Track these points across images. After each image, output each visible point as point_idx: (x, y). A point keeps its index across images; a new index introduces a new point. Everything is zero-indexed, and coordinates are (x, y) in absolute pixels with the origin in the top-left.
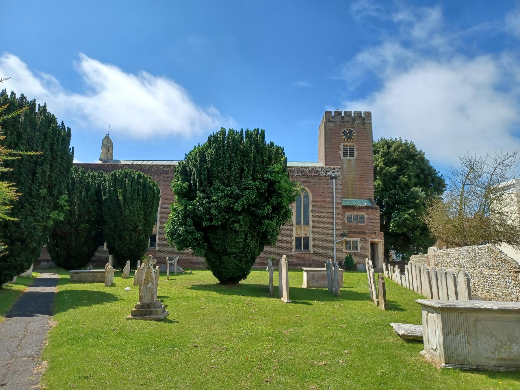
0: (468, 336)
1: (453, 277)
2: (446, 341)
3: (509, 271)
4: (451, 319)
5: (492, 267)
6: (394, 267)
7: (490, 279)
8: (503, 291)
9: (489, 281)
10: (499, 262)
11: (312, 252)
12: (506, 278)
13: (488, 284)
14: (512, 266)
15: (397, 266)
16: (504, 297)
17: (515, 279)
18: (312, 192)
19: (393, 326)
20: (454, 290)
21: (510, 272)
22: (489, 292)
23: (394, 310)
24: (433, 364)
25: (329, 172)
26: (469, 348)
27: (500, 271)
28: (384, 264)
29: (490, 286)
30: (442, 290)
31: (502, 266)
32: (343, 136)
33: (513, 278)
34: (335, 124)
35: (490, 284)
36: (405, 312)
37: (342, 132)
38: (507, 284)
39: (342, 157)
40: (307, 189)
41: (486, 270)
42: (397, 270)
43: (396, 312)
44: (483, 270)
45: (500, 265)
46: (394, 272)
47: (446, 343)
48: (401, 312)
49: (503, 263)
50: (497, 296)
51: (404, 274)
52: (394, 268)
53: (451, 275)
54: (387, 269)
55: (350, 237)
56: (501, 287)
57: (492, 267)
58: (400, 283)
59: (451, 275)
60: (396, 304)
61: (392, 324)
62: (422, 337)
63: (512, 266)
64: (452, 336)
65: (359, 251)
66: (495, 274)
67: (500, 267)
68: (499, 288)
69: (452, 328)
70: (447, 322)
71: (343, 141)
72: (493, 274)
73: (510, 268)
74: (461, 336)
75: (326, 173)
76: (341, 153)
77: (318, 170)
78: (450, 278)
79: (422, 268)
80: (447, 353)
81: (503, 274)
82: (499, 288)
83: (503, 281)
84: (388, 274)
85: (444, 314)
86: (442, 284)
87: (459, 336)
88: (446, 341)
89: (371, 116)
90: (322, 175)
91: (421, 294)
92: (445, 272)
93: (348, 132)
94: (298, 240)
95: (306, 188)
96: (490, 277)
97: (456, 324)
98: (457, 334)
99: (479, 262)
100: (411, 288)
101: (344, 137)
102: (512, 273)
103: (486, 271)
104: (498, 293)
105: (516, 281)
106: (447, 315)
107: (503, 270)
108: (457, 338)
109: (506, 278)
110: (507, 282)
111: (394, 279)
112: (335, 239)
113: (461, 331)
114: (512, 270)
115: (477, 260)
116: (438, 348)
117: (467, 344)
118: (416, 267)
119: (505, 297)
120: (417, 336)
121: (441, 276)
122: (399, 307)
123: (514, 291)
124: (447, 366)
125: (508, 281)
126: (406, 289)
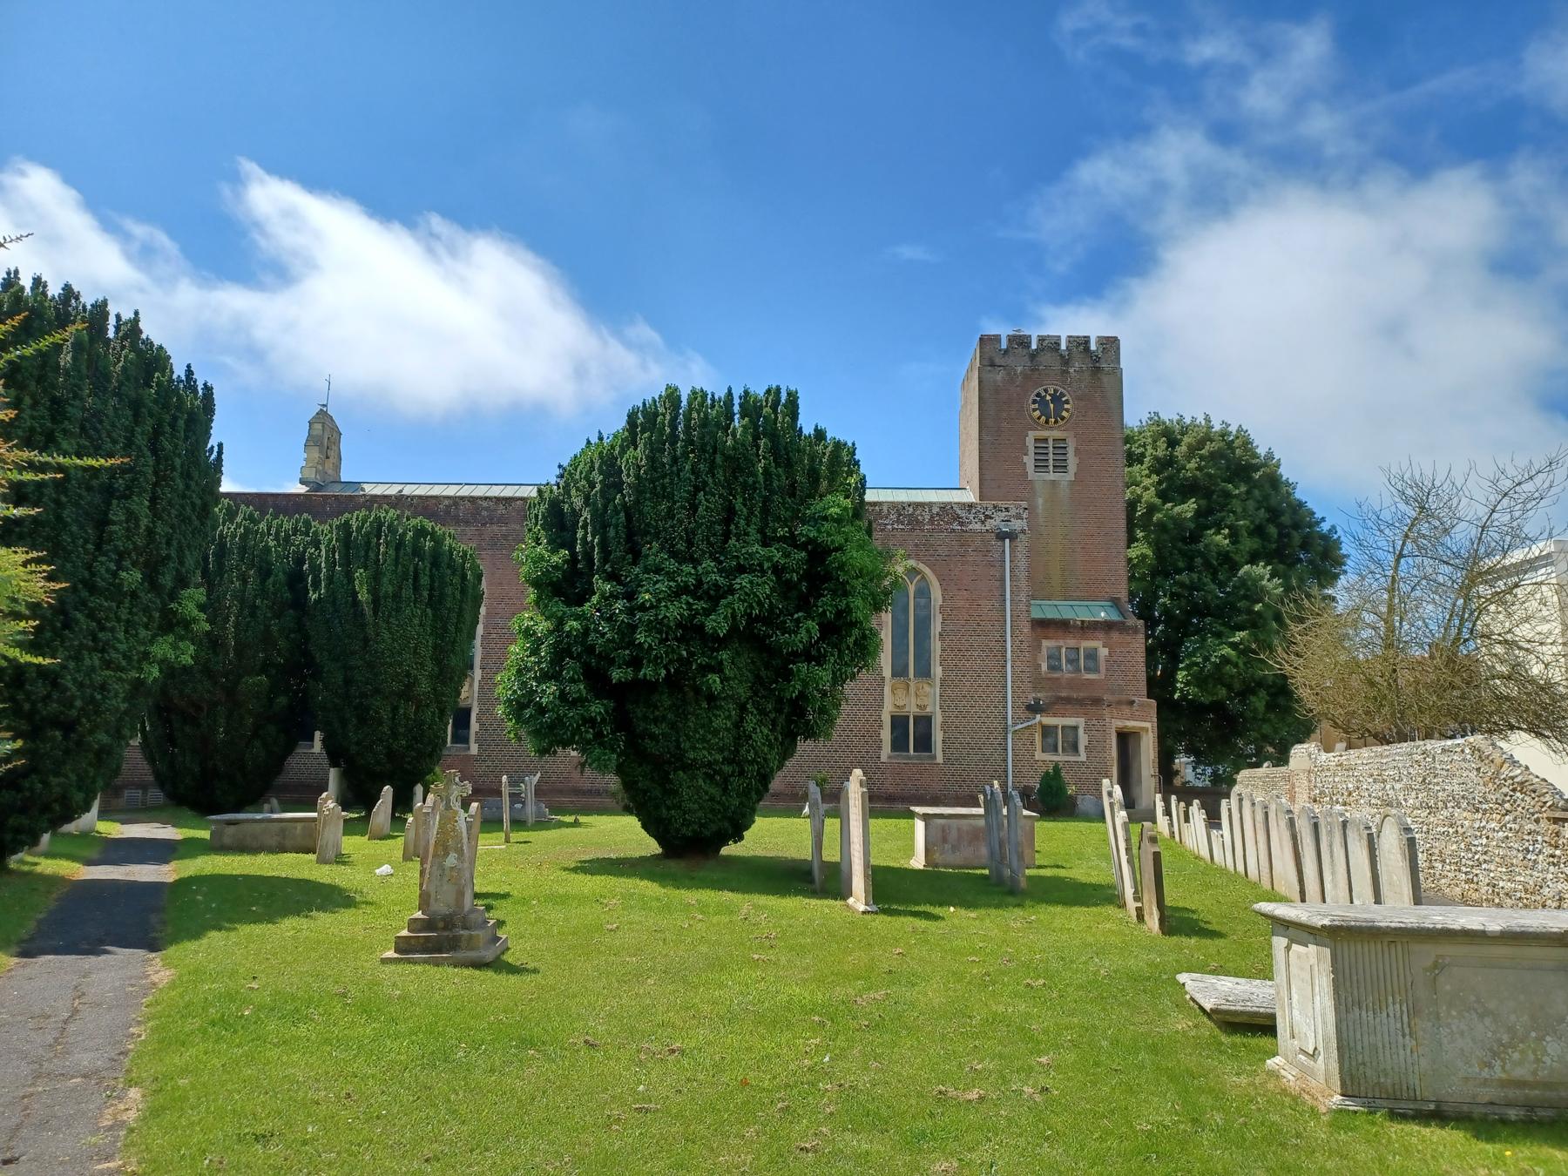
0: (1412, 1012)
1: (1365, 837)
2: (1344, 1028)
3: (1536, 816)
4: (1360, 960)
5: (1484, 806)
6: (1189, 804)
7: (1476, 843)
8: (1518, 878)
9: (1473, 849)
10: (1505, 790)
11: (940, 759)
12: (1526, 837)
13: (1470, 855)
14: (1545, 803)
15: (1196, 802)
16: (1518, 895)
17: (1553, 842)
18: (941, 580)
19: (1184, 984)
20: (1369, 874)
21: (1537, 821)
22: (1475, 879)
23: (1188, 935)
24: (1306, 1097)
25: (992, 518)
26: (1414, 1049)
27: (1507, 818)
28: (1159, 796)
29: (1476, 863)
30: (1333, 873)
31: (1515, 801)
32: (1034, 410)
33: (1546, 839)
34: (1009, 374)
35: (1477, 857)
36: (1222, 940)
37: (1033, 397)
38: (1529, 857)
39: (1031, 473)
40: (927, 571)
41: (1465, 814)
42: (1198, 814)
43: (1193, 941)
44: (1456, 815)
45: (1508, 798)
46: (1187, 820)
47: (1345, 1035)
48: (1208, 942)
49: (1518, 794)
50: (1498, 894)
51: (1219, 826)
52: (1187, 808)
53: (1359, 830)
54: (1168, 812)
55: (1055, 715)
56: (1512, 864)
57: (1484, 806)
58: (1205, 853)
59: (1359, 830)
60: (1195, 917)
61: (1182, 978)
62: (1273, 1017)
63: (1545, 803)
64: (1364, 1013)
65: (1083, 757)
66: (1493, 825)
67: (1507, 806)
68: (1504, 870)
69: (1362, 990)
70: (1347, 971)
71: (1035, 424)
72: (1488, 826)
73: (1537, 809)
74: (1391, 1015)
75: (983, 522)
76: (1029, 460)
77: (959, 512)
78: (1357, 838)
79: (1273, 807)
80: (1346, 1065)
81: (1517, 827)
82: (1504, 870)
83: (1516, 846)
84: (1171, 825)
85: (1339, 947)
86: (1332, 856)
87: (1385, 1014)
88: (1344, 1028)
89: (1119, 349)
90: (970, 527)
91: (1269, 887)
92: (1341, 819)
93: (1048, 398)
94: (899, 723)
95: (922, 566)
96: (1479, 834)
97: (1375, 978)
98: (1377, 1007)
99: (1444, 790)
100: (1241, 868)
101: (1037, 413)
102: (1544, 824)
103: (1465, 819)
104: (1501, 884)
105: (1556, 847)
106: (1349, 949)
107: (1518, 813)
108: (1378, 1020)
109: (1526, 837)
110: (1528, 851)
111: (1189, 842)
112: (1010, 722)
113: (1390, 999)
114: (1545, 815)
115: (1438, 784)
116: (1322, 1050)
117: (1407, 1037)
118: (1253, 804)
119: (1523, 896)
120: (1256, 1014)
121: (1330, 833)
122: (1203, 925)
123: (1551, 876)
124: (1347, 1103)
125: (1531, 848)
126: (1223, 871)
